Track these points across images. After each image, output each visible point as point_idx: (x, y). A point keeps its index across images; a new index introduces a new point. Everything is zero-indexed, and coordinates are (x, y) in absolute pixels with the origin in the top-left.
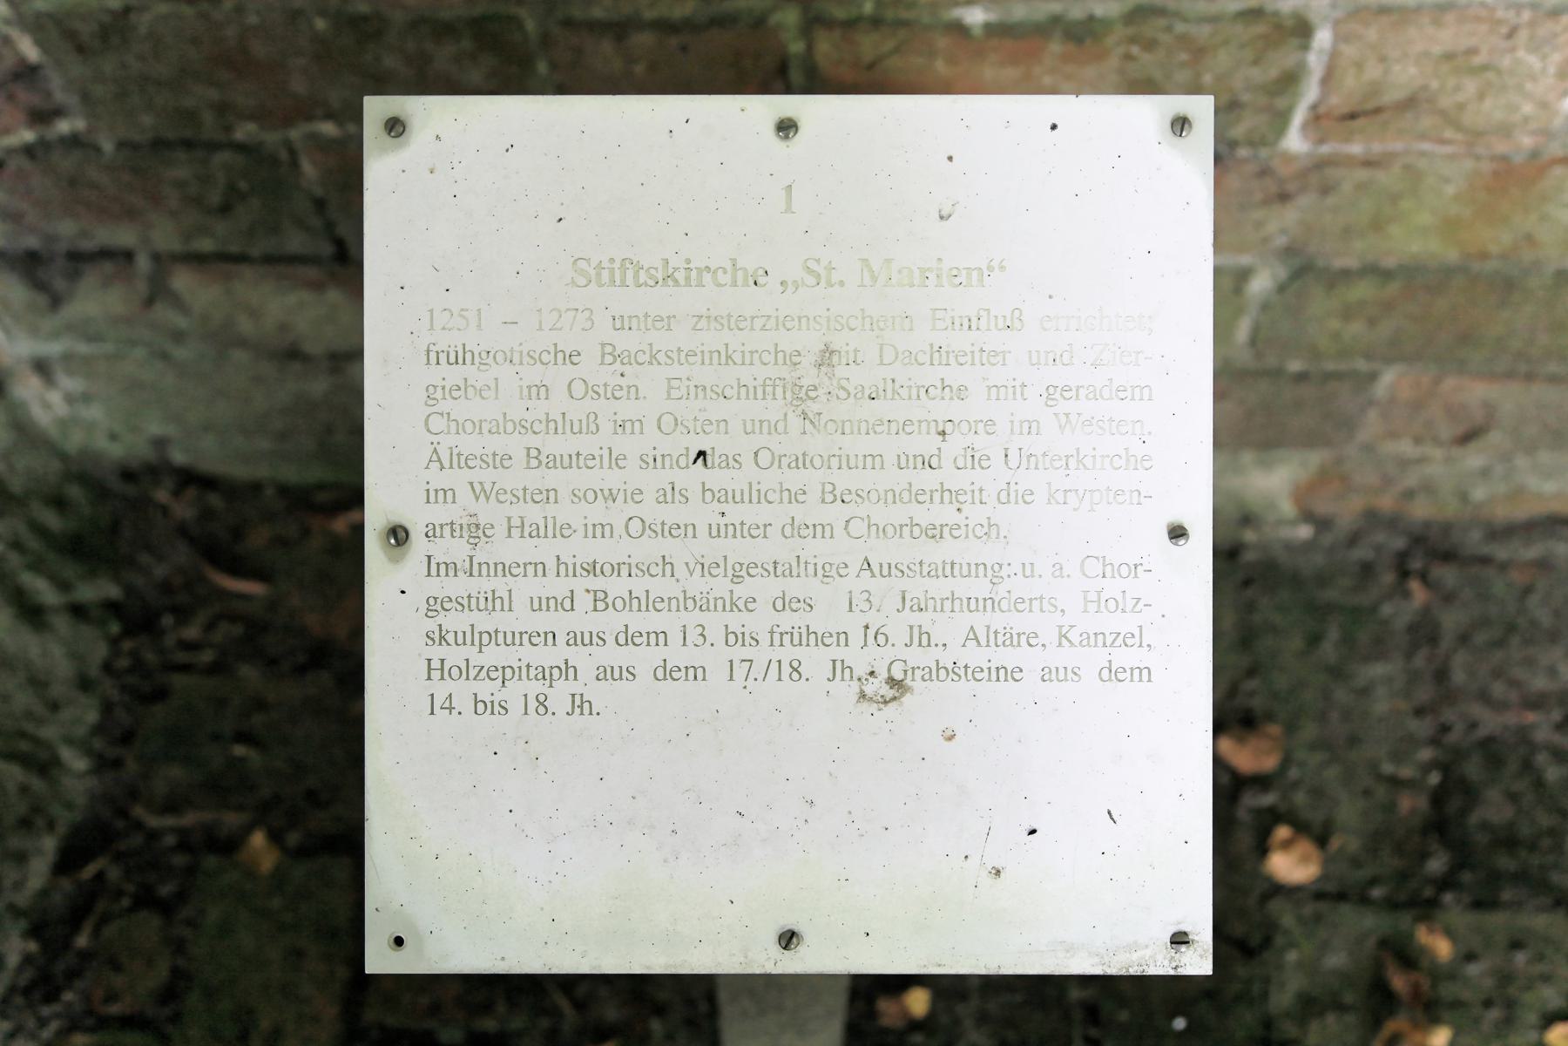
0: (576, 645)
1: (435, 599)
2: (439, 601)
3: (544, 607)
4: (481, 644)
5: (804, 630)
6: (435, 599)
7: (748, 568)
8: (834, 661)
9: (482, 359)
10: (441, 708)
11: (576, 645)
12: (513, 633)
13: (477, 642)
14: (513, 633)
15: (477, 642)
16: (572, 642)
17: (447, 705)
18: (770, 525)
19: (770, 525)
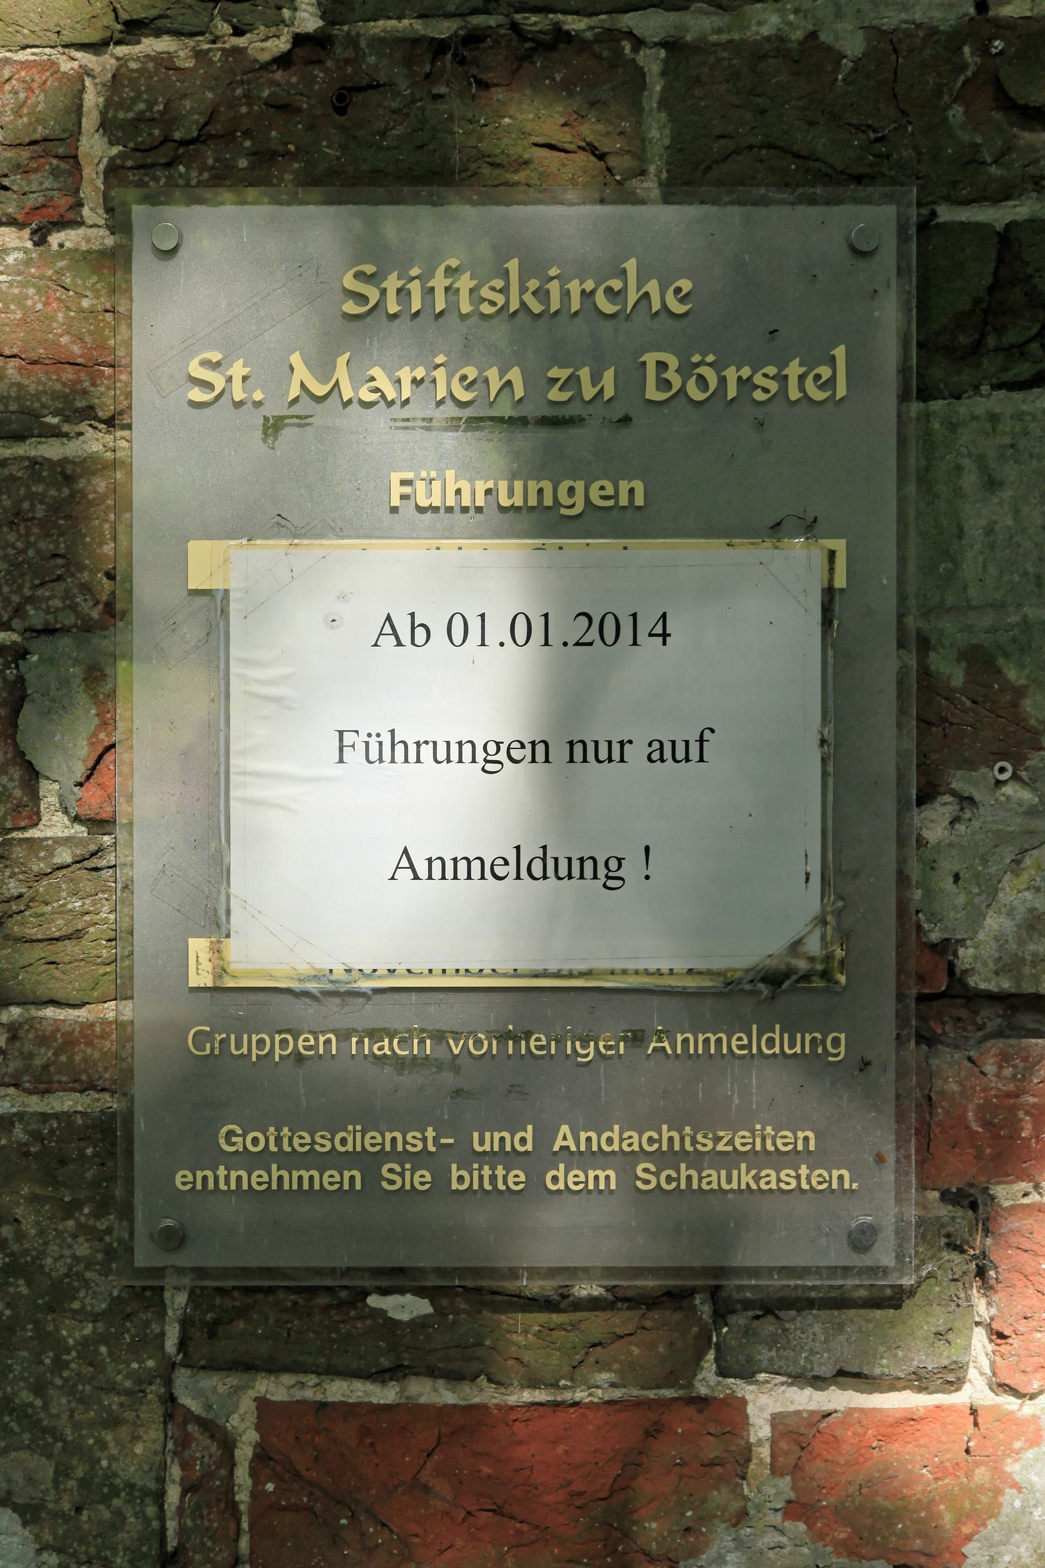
0: (662, 760)
1: (498, 744)
2: (504, 748)
3: (454, 756)
4: (544, 860)
5: (386, 739)
6: (498, 744)
7: (509, 748)
8: (622, 760)
9: (610, 871)
10: (651, 635)
11: (662, 760)
12: (610, 743)
13: (550, 864)
14: (610, 743)
15: (550, 864)
16: (656, 756)
17: (659, 630)
18: (630, 742)
19: (630, 742)
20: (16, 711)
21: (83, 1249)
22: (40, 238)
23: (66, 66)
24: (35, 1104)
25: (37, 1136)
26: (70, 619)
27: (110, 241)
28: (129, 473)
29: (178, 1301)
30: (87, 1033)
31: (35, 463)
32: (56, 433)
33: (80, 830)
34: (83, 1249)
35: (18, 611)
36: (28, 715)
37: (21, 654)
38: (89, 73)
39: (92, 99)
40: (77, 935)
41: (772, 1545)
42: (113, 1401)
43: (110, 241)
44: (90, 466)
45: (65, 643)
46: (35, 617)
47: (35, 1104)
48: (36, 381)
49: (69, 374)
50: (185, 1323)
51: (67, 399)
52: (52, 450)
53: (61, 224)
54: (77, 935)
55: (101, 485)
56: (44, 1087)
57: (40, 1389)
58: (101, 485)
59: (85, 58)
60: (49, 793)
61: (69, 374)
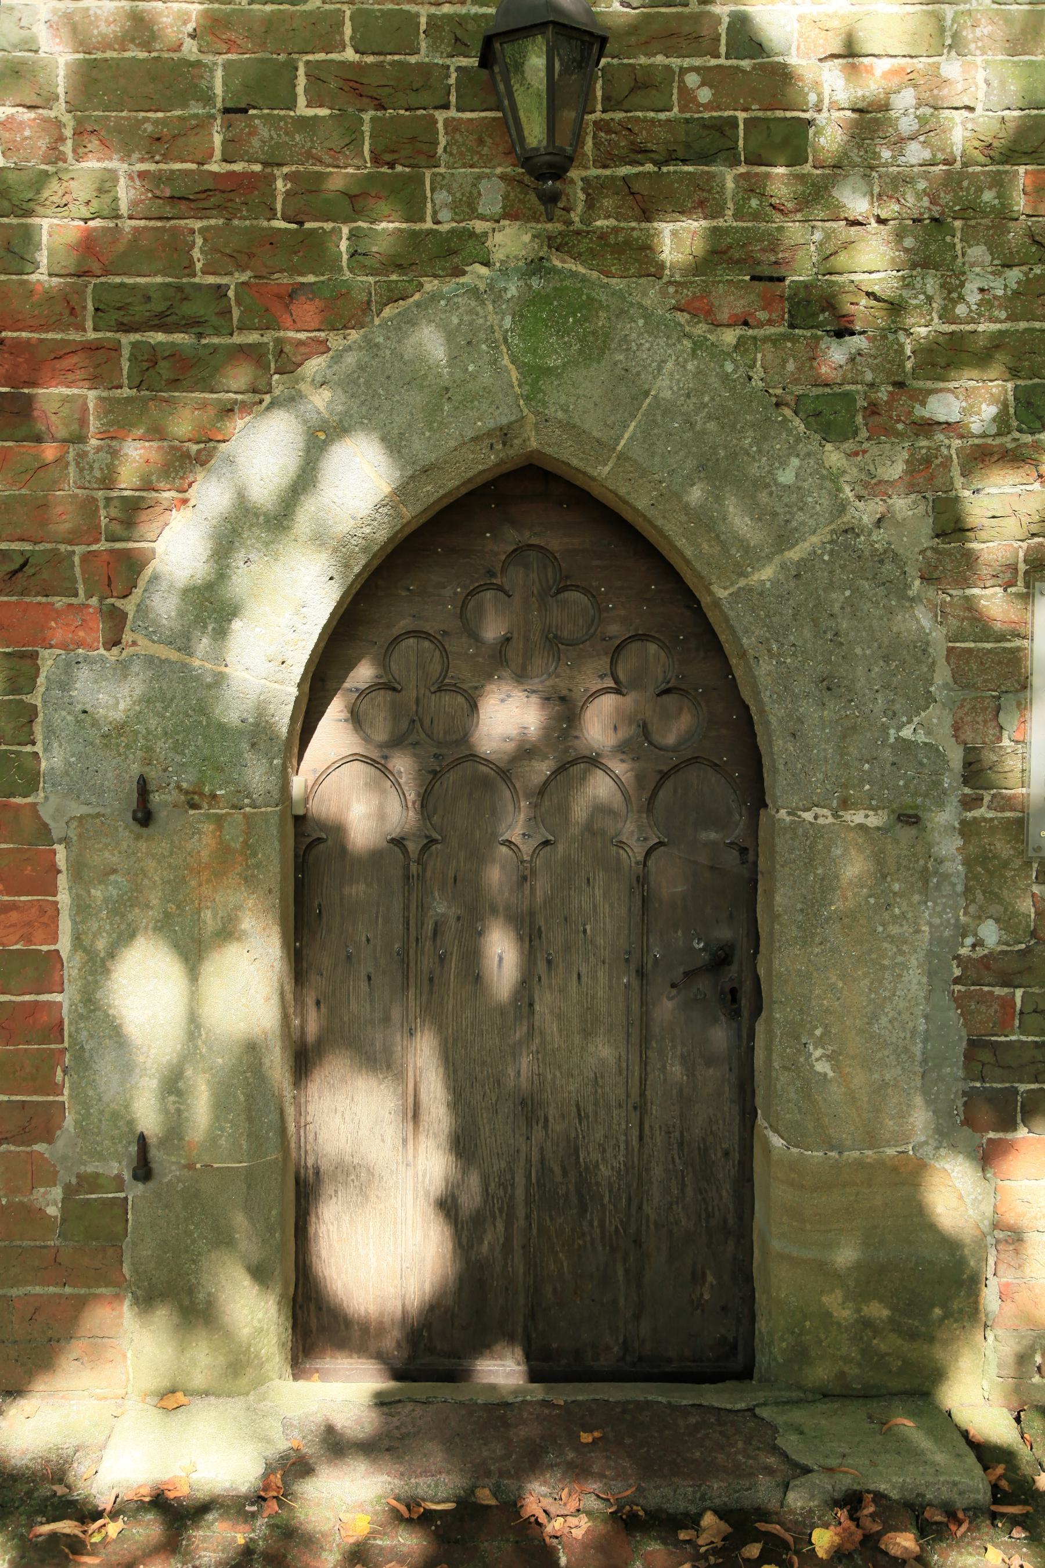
20: (998, 712)
21: (1012, 852)
22: (1005, 590)
23: (1015, 545)
24: (1000, 815)
25: (1000, 823)
26: (1012, 689)
27: (1025, 591)
28: (134, 812)
29: (1035, 866)
30: (1014, 796)
31: (1005, 648)
32: (1009, 640)
33: (1013, 744)
34: (1012, 852)
35: (999, 687)
36: (1001, 715)
37: (999, 698)
38: (1020, 547)
39: (1021, 554)
40: (1012, 771)
41: (400, 1405)
42: (1019, 891)
43: (1025, 591)
44: (1019, 649)
45: (1011, 695)
46: (1004, 688)
47: (1000, 815)
48: (1005, 627)
49: (1013, 625)
50: (1037, 871)
51: (1013, 632)
52: (1008, 645)
53: (1010, 586)
54: (1012, 771)
55: (1021, 654)
56: (1003, 810)
57: (1000, 888)
58: (1021, 654)
59: (1020, 543)
60: (1005, 734)
61: (1013, 625)
